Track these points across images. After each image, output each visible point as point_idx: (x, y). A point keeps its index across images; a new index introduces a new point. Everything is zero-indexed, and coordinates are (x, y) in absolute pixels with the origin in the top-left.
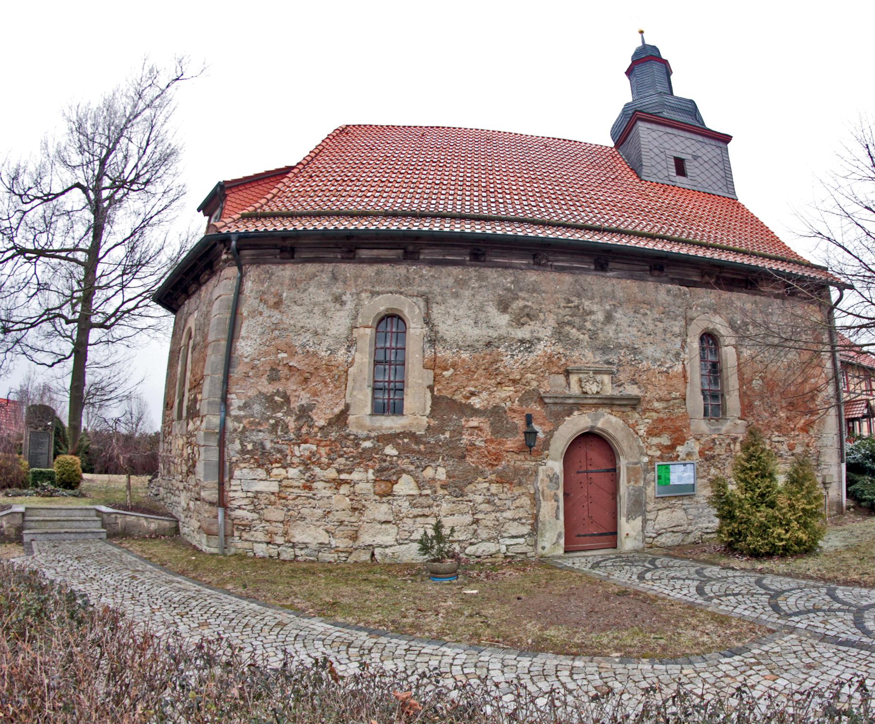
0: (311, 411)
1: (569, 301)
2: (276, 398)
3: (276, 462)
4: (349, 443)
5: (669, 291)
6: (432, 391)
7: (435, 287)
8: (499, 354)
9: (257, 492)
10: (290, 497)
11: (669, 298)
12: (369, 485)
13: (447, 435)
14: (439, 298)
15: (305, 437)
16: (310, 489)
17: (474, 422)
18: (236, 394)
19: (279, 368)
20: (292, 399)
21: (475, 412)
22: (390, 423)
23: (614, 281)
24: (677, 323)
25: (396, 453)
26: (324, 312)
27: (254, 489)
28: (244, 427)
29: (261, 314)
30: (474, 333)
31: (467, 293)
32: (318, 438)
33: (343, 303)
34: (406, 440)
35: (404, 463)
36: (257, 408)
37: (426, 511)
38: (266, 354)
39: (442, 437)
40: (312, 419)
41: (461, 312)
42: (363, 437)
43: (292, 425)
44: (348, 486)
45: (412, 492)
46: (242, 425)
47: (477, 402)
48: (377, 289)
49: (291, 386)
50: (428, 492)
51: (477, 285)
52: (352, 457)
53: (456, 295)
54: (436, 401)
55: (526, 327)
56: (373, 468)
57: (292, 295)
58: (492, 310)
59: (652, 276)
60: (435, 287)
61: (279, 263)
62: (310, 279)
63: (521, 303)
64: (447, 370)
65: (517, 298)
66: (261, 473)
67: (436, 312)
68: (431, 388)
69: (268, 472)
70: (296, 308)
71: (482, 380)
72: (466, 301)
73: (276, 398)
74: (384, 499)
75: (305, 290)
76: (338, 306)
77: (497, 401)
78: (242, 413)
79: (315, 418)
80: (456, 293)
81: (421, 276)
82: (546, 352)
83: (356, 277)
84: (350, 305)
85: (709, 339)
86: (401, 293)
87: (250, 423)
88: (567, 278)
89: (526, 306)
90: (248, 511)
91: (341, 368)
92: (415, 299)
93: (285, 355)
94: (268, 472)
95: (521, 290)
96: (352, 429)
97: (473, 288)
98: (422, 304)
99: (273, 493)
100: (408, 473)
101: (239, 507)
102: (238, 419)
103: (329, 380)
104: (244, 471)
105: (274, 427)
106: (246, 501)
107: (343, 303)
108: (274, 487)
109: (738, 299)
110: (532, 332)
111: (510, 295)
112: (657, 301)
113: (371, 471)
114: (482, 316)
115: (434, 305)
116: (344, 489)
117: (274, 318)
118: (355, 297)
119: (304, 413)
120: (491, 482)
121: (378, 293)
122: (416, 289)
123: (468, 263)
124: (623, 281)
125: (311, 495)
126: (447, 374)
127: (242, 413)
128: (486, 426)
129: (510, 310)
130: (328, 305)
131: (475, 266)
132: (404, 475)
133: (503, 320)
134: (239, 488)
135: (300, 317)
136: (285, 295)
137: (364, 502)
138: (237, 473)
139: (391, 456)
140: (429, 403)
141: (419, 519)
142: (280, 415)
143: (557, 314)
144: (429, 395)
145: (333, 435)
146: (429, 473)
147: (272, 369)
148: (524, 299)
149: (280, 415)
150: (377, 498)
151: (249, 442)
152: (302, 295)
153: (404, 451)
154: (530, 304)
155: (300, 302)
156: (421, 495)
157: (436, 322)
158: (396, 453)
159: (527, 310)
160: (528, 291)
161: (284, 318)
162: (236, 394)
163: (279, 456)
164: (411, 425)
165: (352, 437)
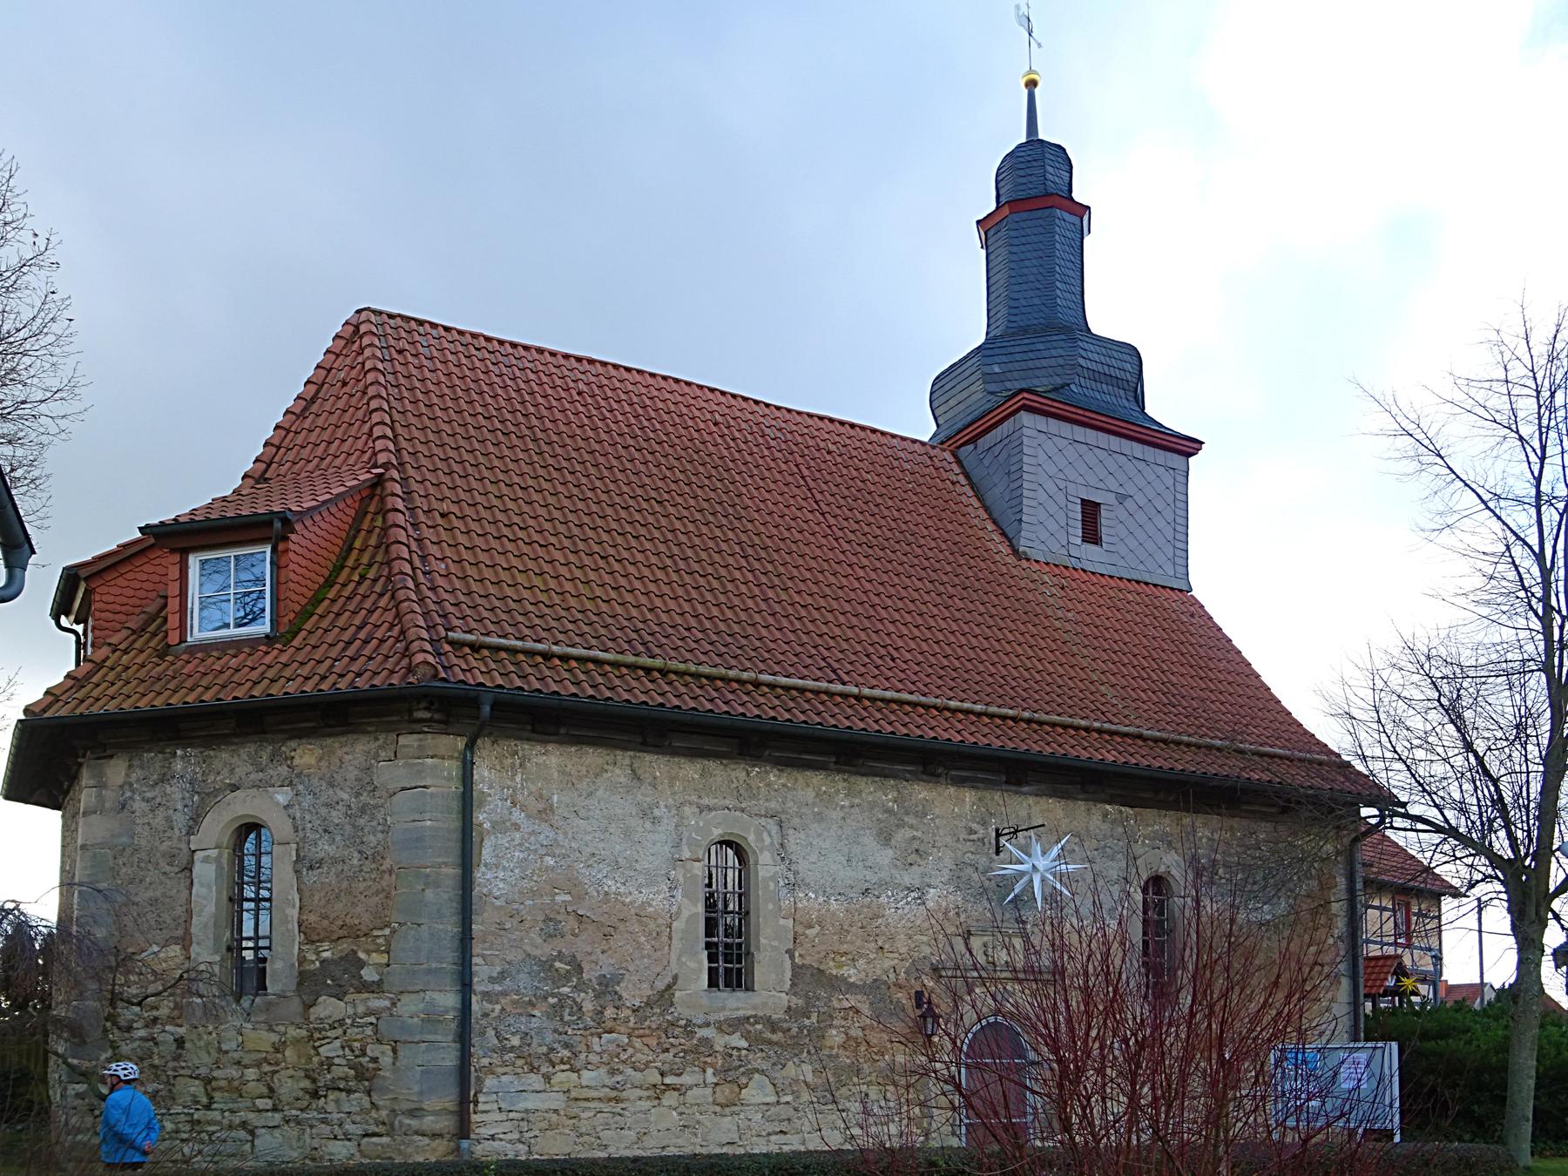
0: (618, 983)
1: (972, 832)
2: (557, 964)
3: (562, 1062)
4: (677, 1031)
5: (1105, 815)
6: (792, 957)
7: (791, 804)
8: (880, 906)
9: (527, 1111)
10: (583, 1115)
11: (1105, 827)
12: (709, 1091)
13: (814, 1018)
14: (796, 821)
15: (609, 1024)
16: (617, 1100)
17: (852, 1000)
18: (483, 956)
19: (559, 918)
20: (586, 966)
21: (852, 988)
22: (734, 1003)
23: (1031, 800)
24: (1114, 864)
25: (746, 1045)
26: (627, 833)
27: (521, 1106)
28: (503, 1009)
29: (517, 827)
30: (846, 875)
31: (836, 814)
32: (631, 1024)
33: (656, 821)
34: (759, 1027)
35: (757, 1061)
36: (523, 980)
37: (784, 1126)
38: (533, 894)
39: (807, 1022)
40: (620, 998)
41: (827, 845)
42: (699, 1022)
43: (588, 1006)
44: (676, 1094)
45: (768, 1100)
46: (498, 1007)
47: (852, 974)
48: (706, 801)
49: (581, 947)
50: (789, 1098)
51: (846, 803)
52: (684, 1051)
53: (819, 817)
54: (797, 971)
55: (915, 867)
56: (712, 1065)
57: (566, 799)
58: (869, 840)
59: (1085, 792)
60: (791, 804)
61: (528, 740)
62: (597, 775)
63: (909, 833)
64: (811, 927)
65: (901, 825)
66: (535, 1081)
67: (794, 841)
68: (790, 953)
69: (547, 1078)
70: (578, 822)
71: (859, 943)
72: (834, 827)
73: (557, 964)
74: (727, 1110)
75: (590, 794)
76: (648, 825)
77: (879, 972)
78: (498, 988)
79: (624, 995)
80: (819, 813)
81: (769, 785)
82: (940, 905)
83: (672, 779)
84: (668, 824)
85: (1157, 883)
86: (743, 811)
87: (514, 1002)
88: (969, 796)
89: (914, 838)
90: (510, 1141)
91: (660, 921)
92: (763, 821)
93: (568, 898)
94: (547, 1078)
95: (907, 813)
96: (681, 1011)
97: (842, 807)
98: (774, 829)
99: (556, 1111)
100: (762, 1072)
101: (493, 1138)
102: (486, 995)
103: (643, 939)
104: (504, 1078)
105: (557, 1009)
106: (508, 1126)
107: (656, 821)
108: (556, 1101)
109: (1205, 825)
110: (923, 875)
111: (893, 820)
112: (1088, 830)
113: (710, 1071)
114: (856, 850)
115: (791, 831)
116: (670, 1099)
117: (542, 837)
118: (674, 812)
119: (607, 988)
120: (869, 1084)
121: (710, 809)
122: (763, 805)
123: (832, 766)
124: (1043, 800)
125: (618, 1110)
126: (811, 932)
127: (498, 988)
128: (865, 1009)
129: (893, 842)
130: (633, 822)
131: (844, 772)
132: (756, 1076)
133: (885, 856)
134: (495, 1106)
135: (588, 838)
136: (555, 798)
137: (698, 1116)
138: (490, 1082)
139: (739, 1049)
140: (788, 974)
141: (773, 1138)
142: (565, 990)
143: (954, 851)
144: (788, 963)
145: (654, 1022)
146: (791, 1070)
147: (548, 919)
148: (911, 827)
149: (565, 990)
150: (718, 1109)
151: (513, 1034)
152: (587, 802)
153: (756, 1042)
154: (919, 834)
155: (582, 813)
156: (778, 1103)
157: (794, 857)
158: (746, 1045)
159: (916, 845)
160: (916, 814)
161: (561, 837)
162: (483, 956)
163: (566, 1053)
164: (765, 1005)
165: (683, 1023)
